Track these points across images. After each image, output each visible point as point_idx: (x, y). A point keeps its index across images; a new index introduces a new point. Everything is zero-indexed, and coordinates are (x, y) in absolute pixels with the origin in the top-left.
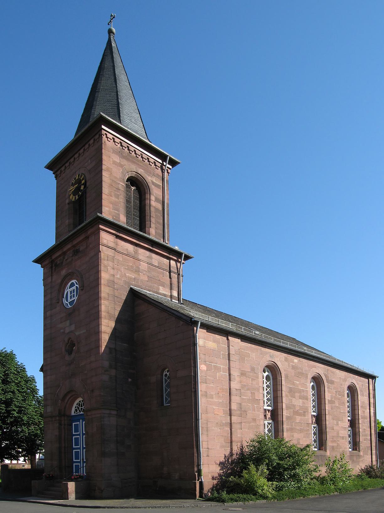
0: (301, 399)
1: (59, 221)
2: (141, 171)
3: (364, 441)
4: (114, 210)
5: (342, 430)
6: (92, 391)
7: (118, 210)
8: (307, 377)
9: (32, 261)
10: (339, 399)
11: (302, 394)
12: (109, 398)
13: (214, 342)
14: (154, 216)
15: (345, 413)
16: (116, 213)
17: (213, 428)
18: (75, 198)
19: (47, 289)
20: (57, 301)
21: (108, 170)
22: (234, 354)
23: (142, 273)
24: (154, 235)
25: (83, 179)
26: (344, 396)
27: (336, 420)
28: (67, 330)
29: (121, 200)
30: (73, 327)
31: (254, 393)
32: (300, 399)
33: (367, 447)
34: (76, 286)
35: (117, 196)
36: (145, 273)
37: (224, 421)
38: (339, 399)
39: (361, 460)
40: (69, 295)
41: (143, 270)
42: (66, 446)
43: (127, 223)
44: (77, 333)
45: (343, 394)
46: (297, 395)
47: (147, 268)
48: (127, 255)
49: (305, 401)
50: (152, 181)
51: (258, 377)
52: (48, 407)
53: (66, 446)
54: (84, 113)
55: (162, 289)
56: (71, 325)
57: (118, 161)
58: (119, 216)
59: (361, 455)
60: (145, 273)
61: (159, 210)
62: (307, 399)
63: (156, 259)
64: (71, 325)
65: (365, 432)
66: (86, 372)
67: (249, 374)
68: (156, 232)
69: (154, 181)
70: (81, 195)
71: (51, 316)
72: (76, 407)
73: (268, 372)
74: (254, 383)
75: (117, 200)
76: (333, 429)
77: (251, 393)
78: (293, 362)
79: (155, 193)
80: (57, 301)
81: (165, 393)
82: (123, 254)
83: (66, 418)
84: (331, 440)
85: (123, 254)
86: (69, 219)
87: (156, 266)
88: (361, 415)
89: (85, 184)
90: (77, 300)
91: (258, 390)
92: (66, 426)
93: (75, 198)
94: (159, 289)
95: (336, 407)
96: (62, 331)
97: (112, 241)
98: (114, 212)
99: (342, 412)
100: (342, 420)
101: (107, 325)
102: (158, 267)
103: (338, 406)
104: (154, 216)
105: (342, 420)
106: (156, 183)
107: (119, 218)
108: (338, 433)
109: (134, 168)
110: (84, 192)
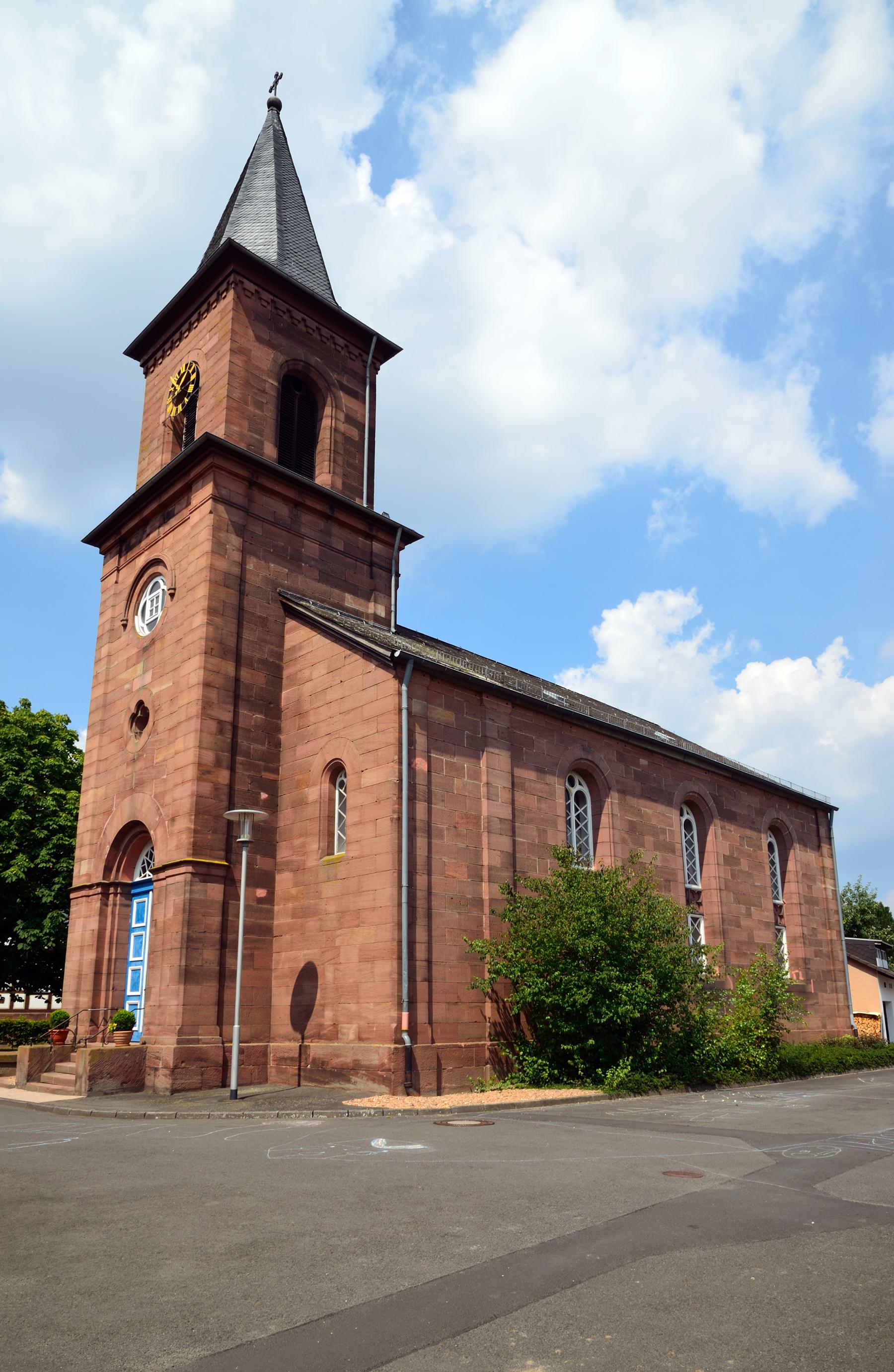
0: (659, 850)
1: (144, 459)
2: (315, 360)
3: (816, 957)
4: (251, 431)
5: (760, 929)
6: (173, 820)
7: (260, 432)
8: (672, 800)
9: (703, 894)
10: (750, 856)
11: (661, 837)
12: (209, 837)
13: (449, 710)
14: (342, 452)
15: (766, 889)
16: (257, 439)
17: (442, 911)
18: (177, 410)
19: (108, 599)
20: (123, 622)
21: (240, 351)
22: (496, 737)
23: (306, 563)
24: (341, 488)
25: (193, 373)
26: (760, 848)
27: (744, 904)
28: (137, 685)
29: (269, 414)
30: (148, 678)
31: (545, 831)
32: (655, 849)
33: (823, 971)
34: (163, 590)
35: (260, 405)
36: (313, 563)
37: (469, 894)
38: (750, 856)
39: (810, 1002)
40: (148, 608)
41: (310, 557)
42: (114, 957)
43: (281, 460)
44: (155, 691)
45: (758, 843)
46: (649, 840)
47: (318, 553)
48: (273, 524)
49: (669, 856)
50: (339, 382)
51: (553, 794)
52: (83, 862)
53: (114, 957)
54: (208, 249)
55: (350, 601)
56: (144, 672)
57: (265, 337)
58: (263, 445)
59: (810, 990)
60: (313, 563)
61: (354, 441)
62: (673, 851)
63: (339, 538)
64: (144, 672)
65: (816, 936)
66: (165, 777)
67: (532, 785)
68: (344, 484)
69: (345, 383)
70: (188, 402)
71: (109, 656)
72: (143, 863)
73: (580, 784)
74: (544, 806)
75: (258, 412)
76: (739, 926)
77: (538, 830)
78: (638, 765)
79: (346, 406)
80: (123, 622)
81: (339, 824)
82: (264, 520)
83: (119, 890)
84: (736, 951)
85: (264, 520)
86: (163, 453)
87: (338, 551)
88: (804, 896)
89: (197, 382)
90: (163, 617)
91: (555, 824)
92: (118, 907)
93: (177, 410)
94: (344, 600)
95: (744, 872)
96: (127, 686)
97: (240, 491)
98: (252, 437)
99: (757, 886)
100: (759, 905)
101: (215, 669)
102: (344, 553)
103: (747, 872)
104: (342, 452)
105: (759, 905)
106: (347, 387)
107: (262, 449)
108: (751, 935)
109: (300, 353)
110: (194, 399)
